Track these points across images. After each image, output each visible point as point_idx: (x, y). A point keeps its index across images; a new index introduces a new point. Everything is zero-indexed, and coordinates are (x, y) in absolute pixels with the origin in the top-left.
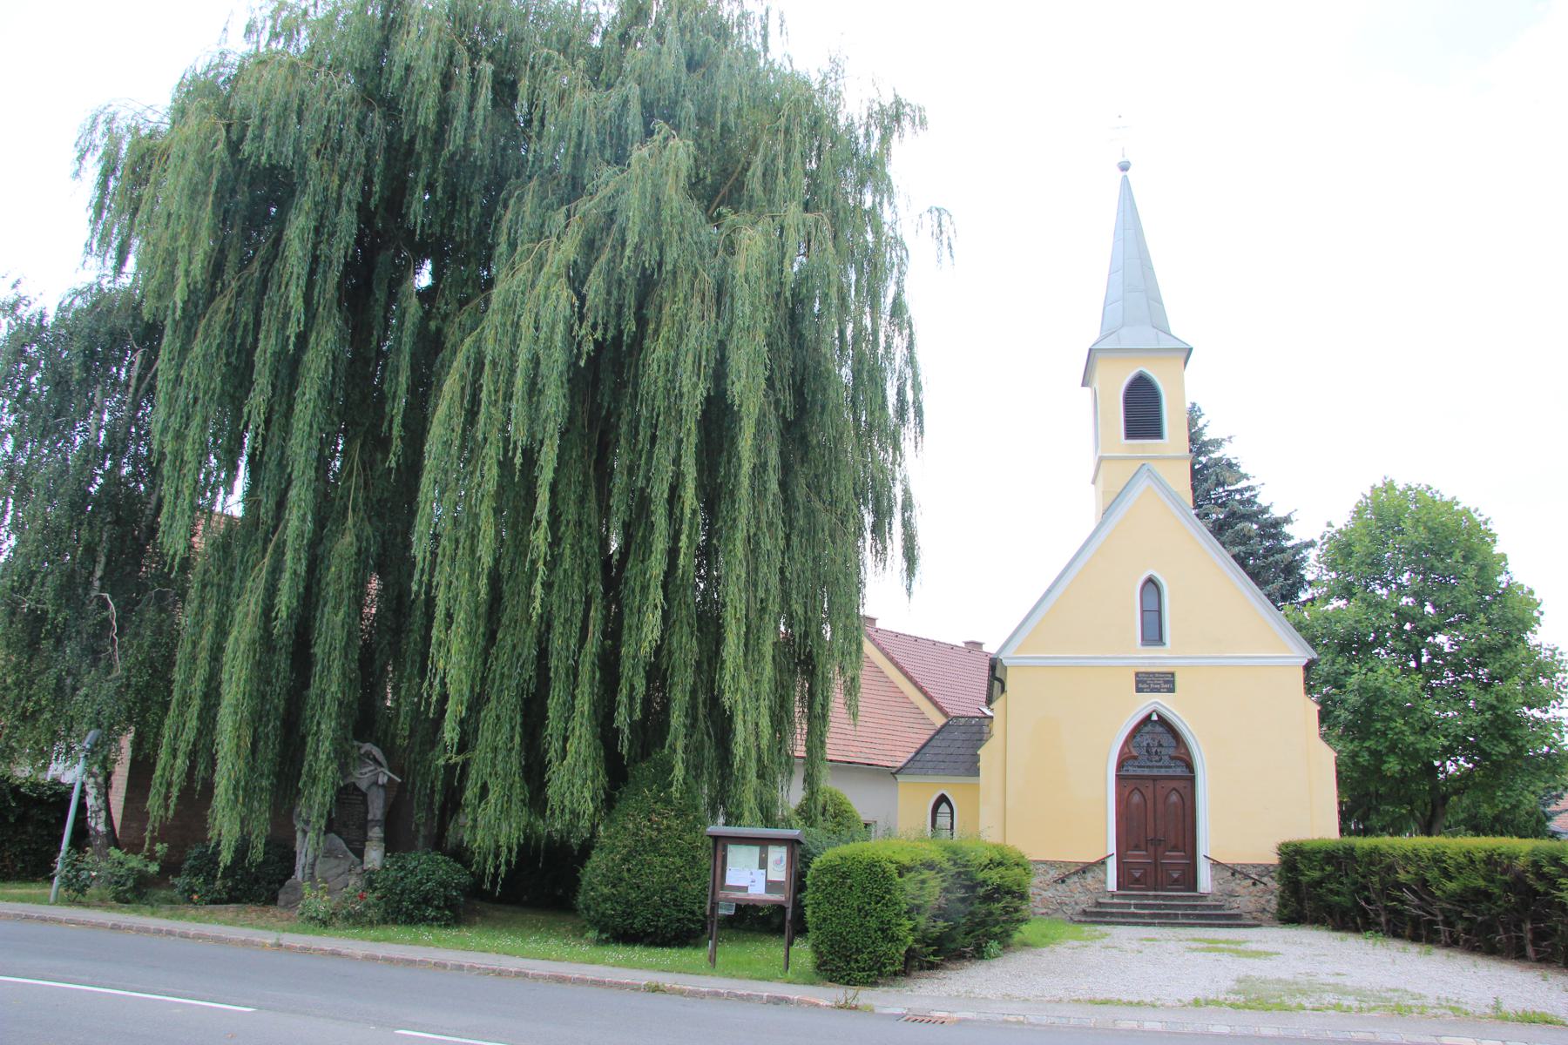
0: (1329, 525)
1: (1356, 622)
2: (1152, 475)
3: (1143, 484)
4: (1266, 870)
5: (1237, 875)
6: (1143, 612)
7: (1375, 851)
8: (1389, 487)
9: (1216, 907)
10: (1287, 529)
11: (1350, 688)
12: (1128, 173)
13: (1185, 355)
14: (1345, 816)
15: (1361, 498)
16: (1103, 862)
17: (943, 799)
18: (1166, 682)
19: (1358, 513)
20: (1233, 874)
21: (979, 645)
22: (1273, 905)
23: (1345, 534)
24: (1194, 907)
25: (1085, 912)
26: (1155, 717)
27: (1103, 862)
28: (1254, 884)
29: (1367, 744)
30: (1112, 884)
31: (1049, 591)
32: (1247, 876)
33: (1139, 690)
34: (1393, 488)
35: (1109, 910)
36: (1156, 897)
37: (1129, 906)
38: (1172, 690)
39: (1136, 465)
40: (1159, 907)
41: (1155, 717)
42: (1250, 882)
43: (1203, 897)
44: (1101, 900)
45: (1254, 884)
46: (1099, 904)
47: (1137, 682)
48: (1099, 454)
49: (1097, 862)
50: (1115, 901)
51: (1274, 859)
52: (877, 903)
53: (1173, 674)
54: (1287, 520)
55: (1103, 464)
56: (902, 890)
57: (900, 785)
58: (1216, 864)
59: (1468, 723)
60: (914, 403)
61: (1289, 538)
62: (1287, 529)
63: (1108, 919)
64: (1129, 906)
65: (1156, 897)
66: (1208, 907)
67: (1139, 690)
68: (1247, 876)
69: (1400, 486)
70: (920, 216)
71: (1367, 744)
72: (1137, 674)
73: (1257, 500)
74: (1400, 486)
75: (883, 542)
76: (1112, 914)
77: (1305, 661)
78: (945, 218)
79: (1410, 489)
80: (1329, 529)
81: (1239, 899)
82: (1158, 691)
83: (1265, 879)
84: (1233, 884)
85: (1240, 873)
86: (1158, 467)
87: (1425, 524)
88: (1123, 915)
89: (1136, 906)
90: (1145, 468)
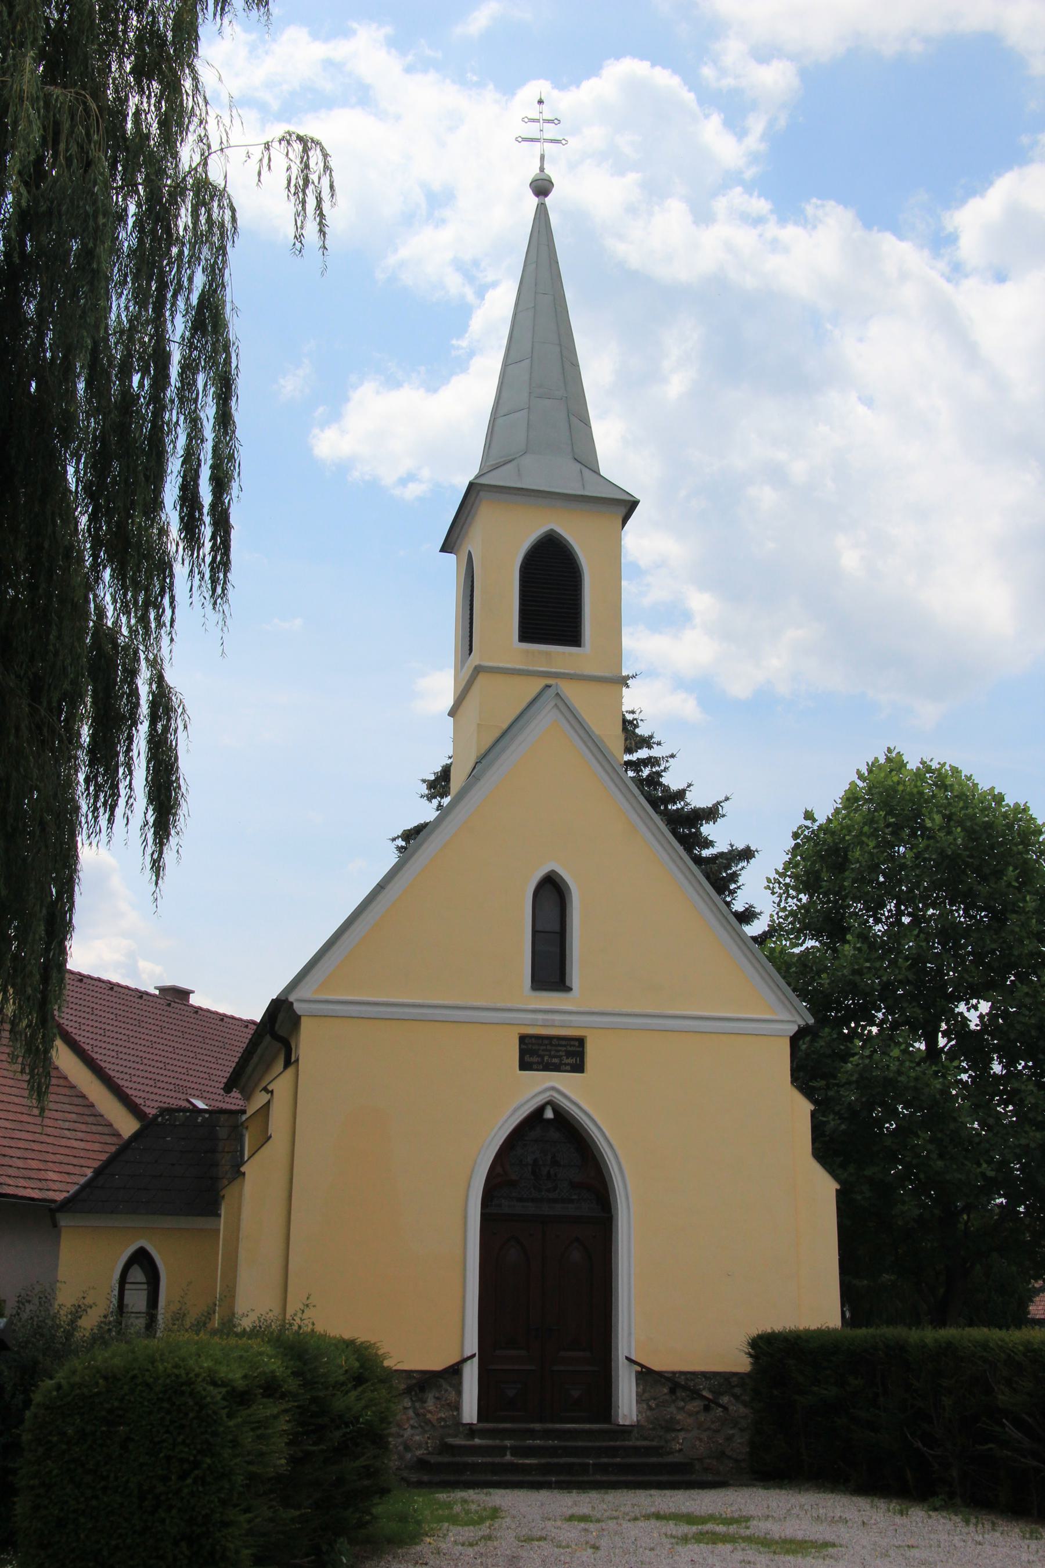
0: (809, 816)
1: (854, 972)
2: (563, 704)
3: (547, 718)
4: (724, 1381)
5: (680, 1393)
6: (535, 932)
7: (948, 1349)
8: (895, 763)
9: (649, 1451)
10: (707, 829)
11: (842, 1078)
12: (548, 200)
13: (623, 511)
14: (848, 1294)
15: (855, 778)
16: (455, 1371)
17: (141, 1259)
18: (569, 1054)
19: (851, 799)
20: (672, 1391)
21: (183, 994)
22: (740, 1444)
23: (833, 833)
24: (613, 1451)
25: (422, 1465)
26: (549, 1114)
27: (455, 1371)
28: (707, 1409)
29: (868, 1172)
30: (470, 1411)
31: (380, 887)
32: (695, 1394)
33: (524, 1066)
34: (903, 765)
35: (470, 1460)
36: (547, 1434)
37: (501, 1451)
38: (579, 1067)
39: (535, 686)
40: (553, 1452)
41: (549, 1114)
42: (695, 1405)
43: (625, 1431)
44: (451, 1441)
45: (707, 1409)
46: (447, 1448)
47: (522, 1053)
48: (475, 660)
49: (445, 1371)
50: (477, 1441)
51: (742, 1364)
52: (183, 1477)
53: (581, 1041)
54: (711, 814)
55: (482, 679)
56: (235, 1443)
57: (64, 1236)
58: (646, 1376)
59: (1023, 1141)
60: (213, 506)
61: (708, 844)
62: (707, 829)
63: (467, 1477)
64: (501, 1451)
65: (547, 1434)
66: (636, 1451)
67: (524, 1066)
68: (695, 1394)
69: (913, 764)
70: (267, 146)
71: (868, 1172)
72: (523, 1039)
73: (664, 780)
74: (913, 764)
75: (112, 773)
76: (474, 1468)
77: (794, 1028)
78: (315, 158)
79: (929, 770)
80: (808, 823)
81: (682, 1435)
82: (557, 1068)
83: (725, 1400)
84: (672, 1409)
85: (685, 1388)
86: (568, 689)
87: (960, 823)
88: (495, 1469)
89: (516, 1451)
90: (551, 692)
